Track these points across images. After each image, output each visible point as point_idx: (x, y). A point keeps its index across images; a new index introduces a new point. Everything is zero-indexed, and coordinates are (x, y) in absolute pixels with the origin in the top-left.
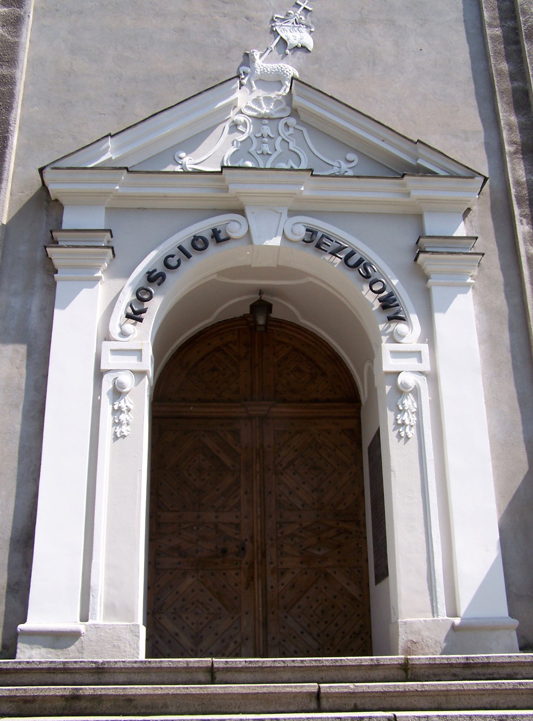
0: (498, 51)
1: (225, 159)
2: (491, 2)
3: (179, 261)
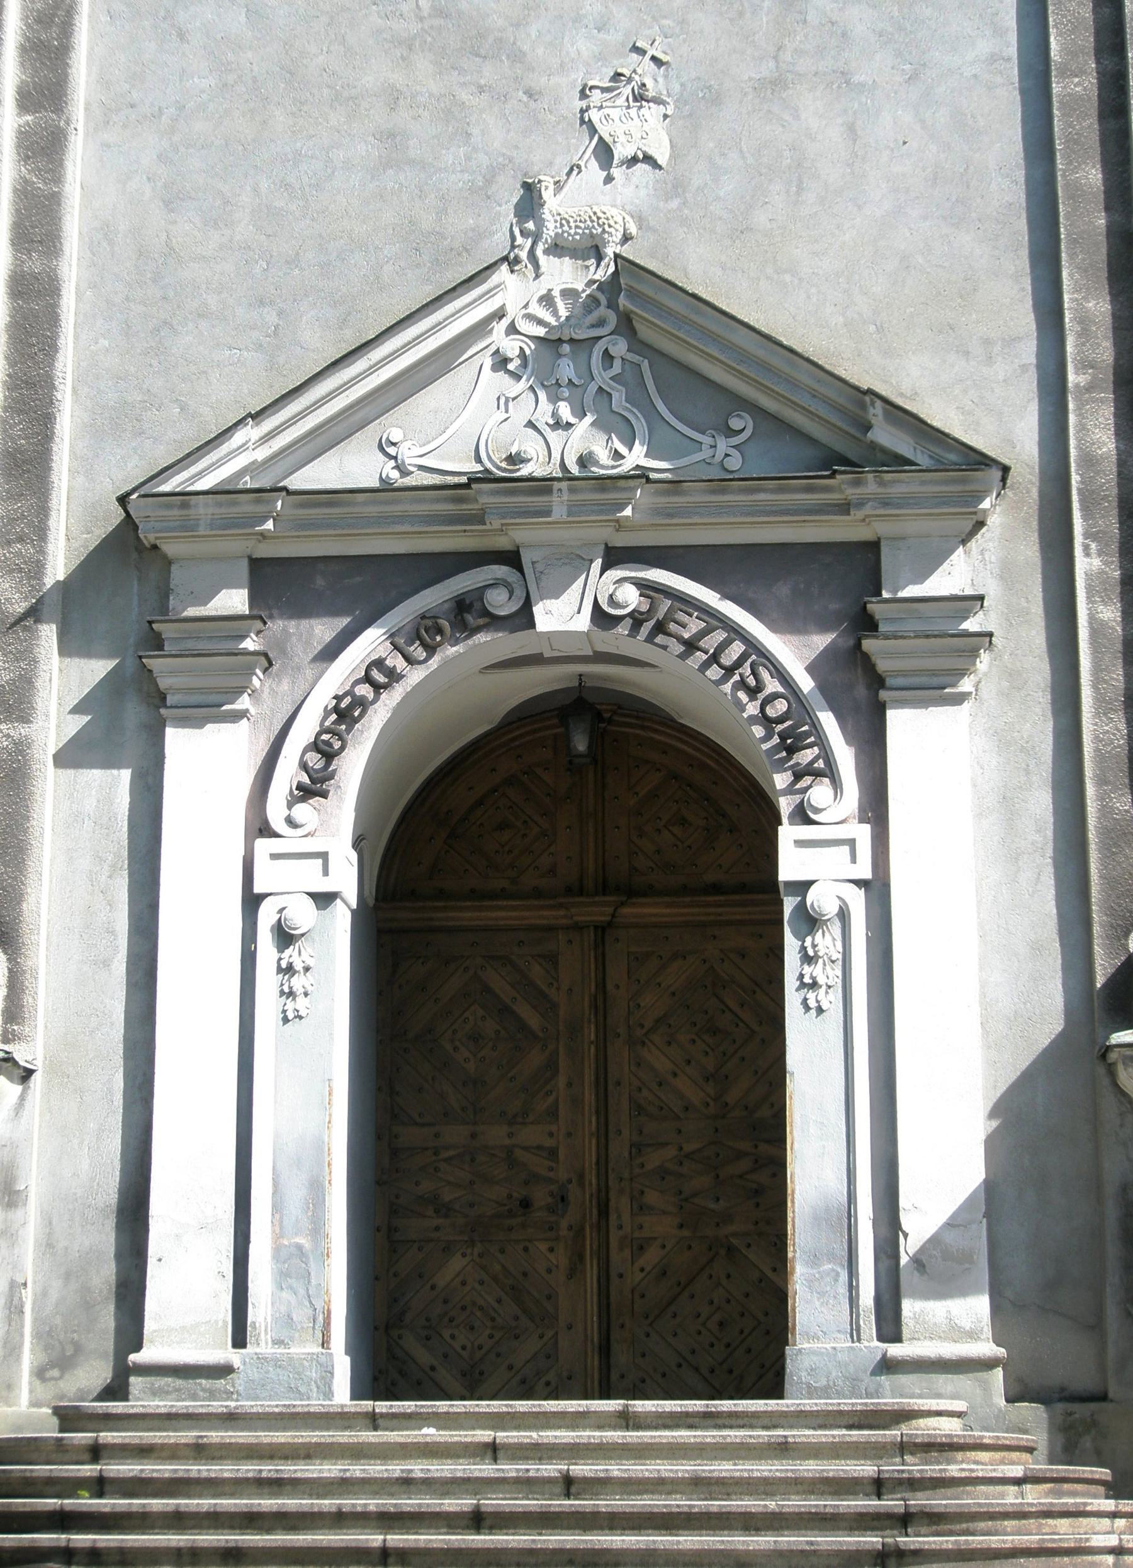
0: (1076, 137)
2: (1069, 11)
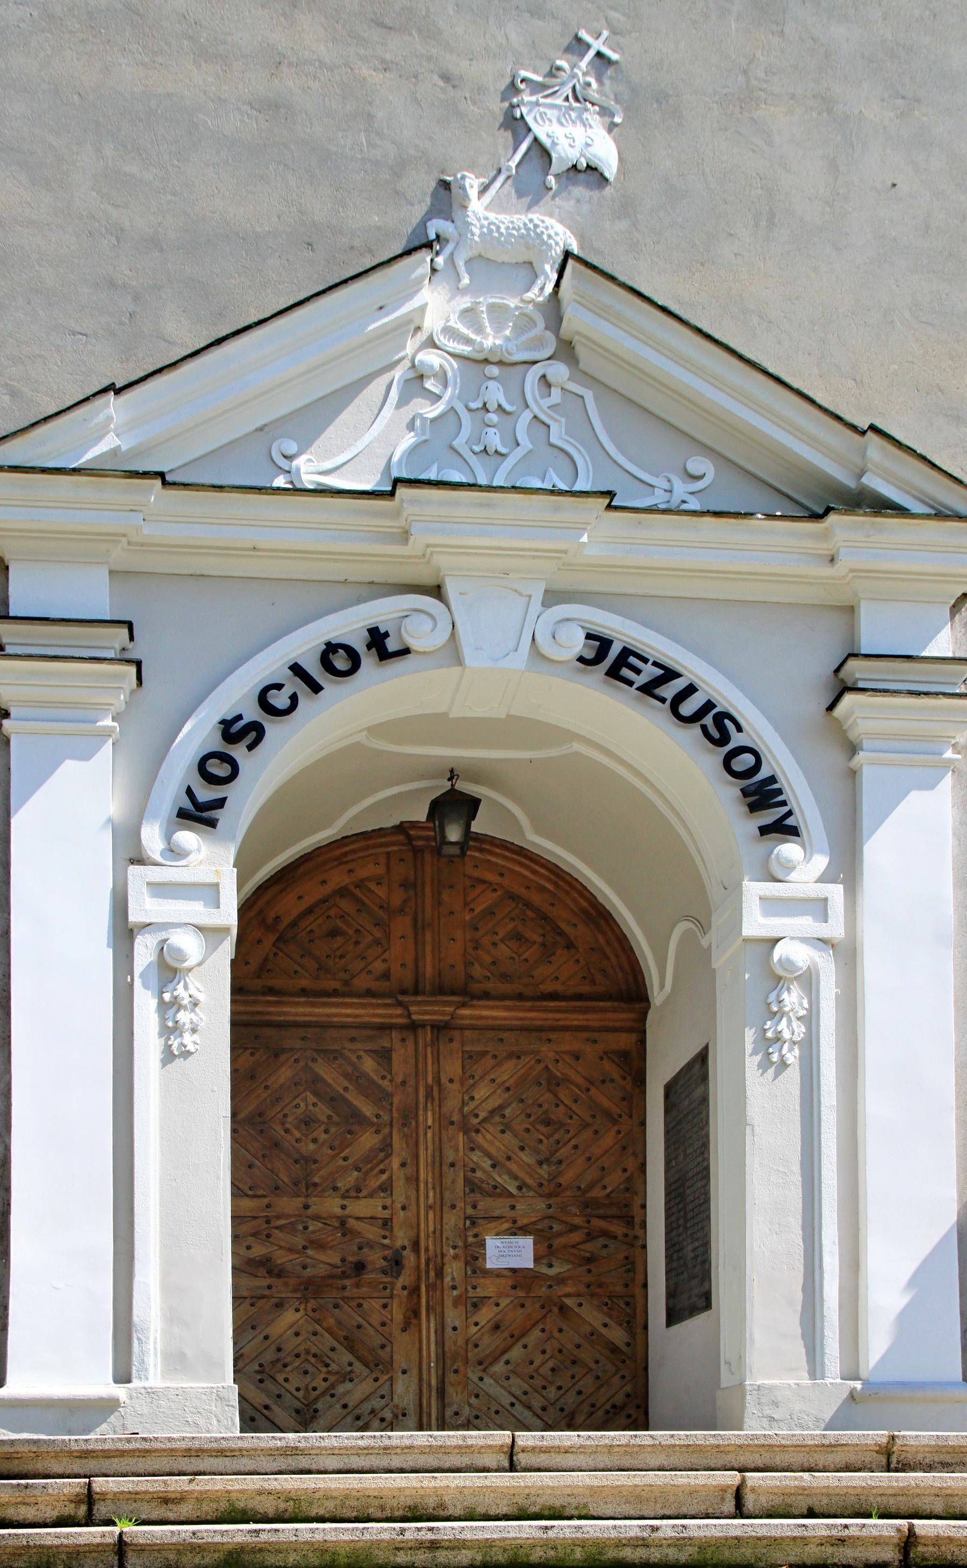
1: (396, 458)
3: (294, 698)
